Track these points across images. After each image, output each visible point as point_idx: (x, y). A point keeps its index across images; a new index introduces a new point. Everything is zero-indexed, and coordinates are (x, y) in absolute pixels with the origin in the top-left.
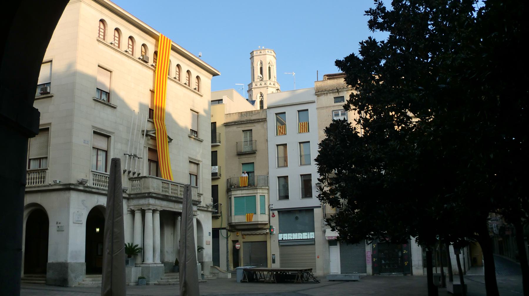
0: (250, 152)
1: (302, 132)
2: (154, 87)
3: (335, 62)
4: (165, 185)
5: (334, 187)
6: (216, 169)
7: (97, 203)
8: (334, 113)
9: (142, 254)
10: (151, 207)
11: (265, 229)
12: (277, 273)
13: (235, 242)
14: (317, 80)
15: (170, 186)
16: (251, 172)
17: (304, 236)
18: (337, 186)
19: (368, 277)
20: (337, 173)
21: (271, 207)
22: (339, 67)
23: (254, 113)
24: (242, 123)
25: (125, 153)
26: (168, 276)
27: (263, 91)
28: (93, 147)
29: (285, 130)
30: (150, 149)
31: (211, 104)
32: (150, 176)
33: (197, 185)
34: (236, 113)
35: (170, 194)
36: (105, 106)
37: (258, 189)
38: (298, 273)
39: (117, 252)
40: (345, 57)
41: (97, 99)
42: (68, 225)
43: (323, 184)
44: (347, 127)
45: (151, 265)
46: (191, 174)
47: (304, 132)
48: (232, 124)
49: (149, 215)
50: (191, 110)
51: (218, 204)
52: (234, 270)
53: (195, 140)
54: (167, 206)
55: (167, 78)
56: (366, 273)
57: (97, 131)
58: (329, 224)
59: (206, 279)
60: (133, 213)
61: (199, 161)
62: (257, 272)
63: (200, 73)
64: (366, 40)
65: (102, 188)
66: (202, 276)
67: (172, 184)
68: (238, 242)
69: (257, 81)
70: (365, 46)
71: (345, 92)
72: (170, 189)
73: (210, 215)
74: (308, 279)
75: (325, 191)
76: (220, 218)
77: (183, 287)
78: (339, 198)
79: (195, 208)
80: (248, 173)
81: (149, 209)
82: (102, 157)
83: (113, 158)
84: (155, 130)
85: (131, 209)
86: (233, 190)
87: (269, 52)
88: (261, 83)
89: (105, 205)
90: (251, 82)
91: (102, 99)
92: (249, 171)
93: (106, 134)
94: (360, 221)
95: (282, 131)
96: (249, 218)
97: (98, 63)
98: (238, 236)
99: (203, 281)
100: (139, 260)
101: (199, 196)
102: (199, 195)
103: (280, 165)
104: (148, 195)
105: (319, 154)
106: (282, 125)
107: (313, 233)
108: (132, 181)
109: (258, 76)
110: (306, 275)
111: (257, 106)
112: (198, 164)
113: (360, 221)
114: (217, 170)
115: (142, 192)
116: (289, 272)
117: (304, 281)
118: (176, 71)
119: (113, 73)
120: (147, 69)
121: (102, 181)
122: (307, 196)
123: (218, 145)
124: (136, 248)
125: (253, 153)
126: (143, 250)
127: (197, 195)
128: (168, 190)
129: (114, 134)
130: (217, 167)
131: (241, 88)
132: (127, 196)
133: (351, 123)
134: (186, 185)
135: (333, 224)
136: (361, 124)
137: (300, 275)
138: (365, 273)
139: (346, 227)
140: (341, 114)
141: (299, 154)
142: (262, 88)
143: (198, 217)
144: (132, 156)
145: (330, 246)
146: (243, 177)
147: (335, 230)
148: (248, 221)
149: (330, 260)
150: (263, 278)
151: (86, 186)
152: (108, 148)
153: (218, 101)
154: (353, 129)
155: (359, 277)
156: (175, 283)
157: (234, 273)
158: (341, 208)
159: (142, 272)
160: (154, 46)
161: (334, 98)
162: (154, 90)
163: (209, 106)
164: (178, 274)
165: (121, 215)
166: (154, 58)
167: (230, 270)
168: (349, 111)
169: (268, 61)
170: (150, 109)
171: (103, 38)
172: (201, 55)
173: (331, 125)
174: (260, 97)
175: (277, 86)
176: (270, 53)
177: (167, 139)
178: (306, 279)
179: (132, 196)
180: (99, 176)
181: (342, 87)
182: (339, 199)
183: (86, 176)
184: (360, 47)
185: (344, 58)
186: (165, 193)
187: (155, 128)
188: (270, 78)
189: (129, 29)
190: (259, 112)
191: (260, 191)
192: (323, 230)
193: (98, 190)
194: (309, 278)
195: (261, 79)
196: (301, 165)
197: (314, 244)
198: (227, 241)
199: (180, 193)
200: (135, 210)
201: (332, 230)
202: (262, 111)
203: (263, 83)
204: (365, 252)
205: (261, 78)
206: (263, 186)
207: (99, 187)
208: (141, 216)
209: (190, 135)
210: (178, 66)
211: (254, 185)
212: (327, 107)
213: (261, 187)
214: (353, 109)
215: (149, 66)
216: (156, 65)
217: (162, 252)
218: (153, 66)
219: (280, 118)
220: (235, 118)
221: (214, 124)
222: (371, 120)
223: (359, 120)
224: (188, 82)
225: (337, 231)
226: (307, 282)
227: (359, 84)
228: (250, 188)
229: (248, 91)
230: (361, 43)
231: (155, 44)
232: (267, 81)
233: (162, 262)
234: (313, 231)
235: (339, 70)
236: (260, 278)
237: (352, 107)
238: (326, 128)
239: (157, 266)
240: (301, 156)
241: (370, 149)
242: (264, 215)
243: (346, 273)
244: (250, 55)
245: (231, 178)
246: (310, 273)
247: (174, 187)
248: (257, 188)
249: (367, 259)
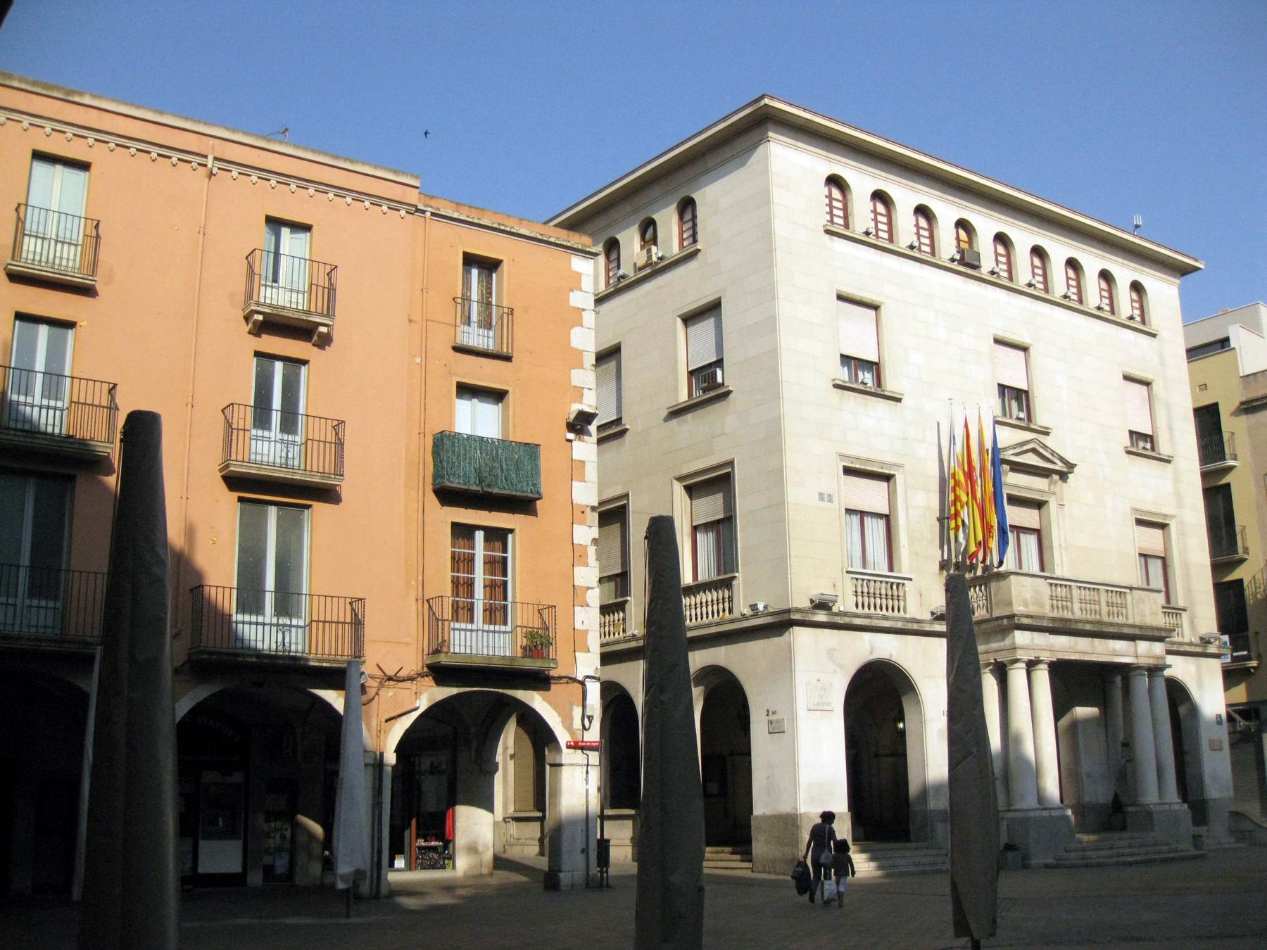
7: (871, 653)
15: (1075, 592)
35: (1078, 615)
42: (793, 718)
45: (1031, 814)
49: (1018, 676)
57: (853, 466)
61: (1165, 516)
65: (881, 613)
67: (1080, 588)
72: (1075, 600)
97: (993, 334)
101: (1177, 614)
102: (1177, 611)
123: (1231, 468)
128: (1097, 607)
129: (902, 469)
183: (834, 586)
186: (1085, 616)
239: (1050, 816)
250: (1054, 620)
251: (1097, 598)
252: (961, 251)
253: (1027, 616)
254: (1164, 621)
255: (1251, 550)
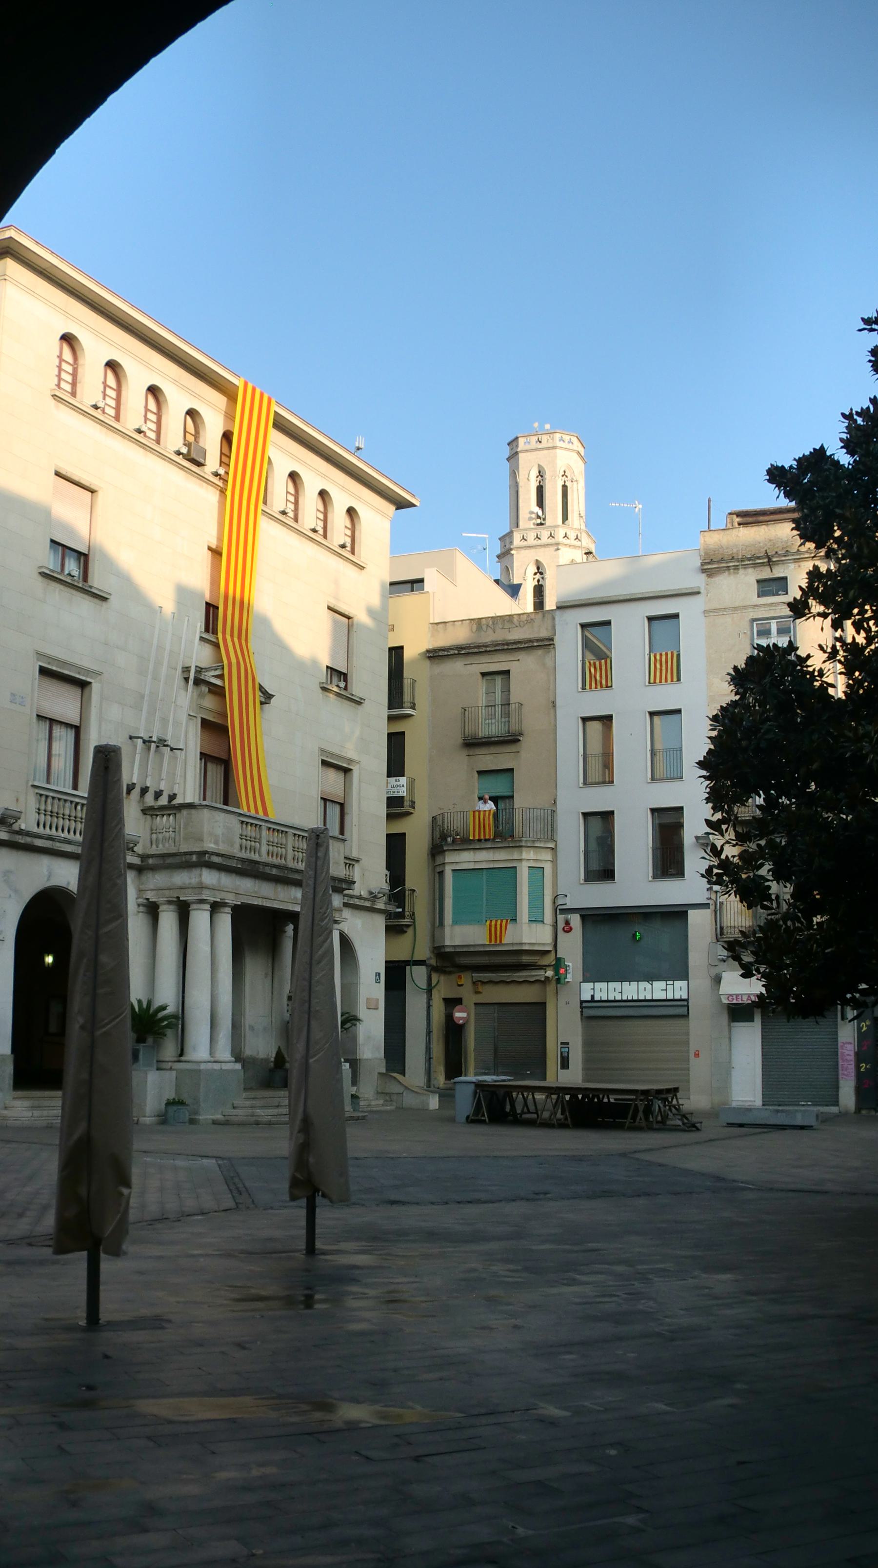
0: (501, 739)
1: (658, 680)
2: (220, 539)
3: (767, 471)
4: (250, 831)
5: (752, 846)
6: (401, 786)
7: (48, 880)
8: (755, 625)
9: (178, 1030)
10: (206, 895)
11: (543, 967)
12: (574, 1096)
13: (452, 1003)
14: (709, 528)
15: (265, 832)
16: (503, 798)
17: (658, 990)
18: (763, 843)
19: (843, 1116)
20: (761, 805)
21: (560, 901)
22: (778, 486)
23: (515, 619)
24: (481, 650)
25: (133, 735)
26: (253, 1098)
27: (544, 556)
28: (38, 716)
29: (608, 673)
30: (205, 723)
31: (390, 594)
32: (204, 803)
33: (342, 832)
34: (462, 621)
35: (264, 858)
36: (74, 592)
37: (523, 848)
38: (635, 1100)
39: (107, 1024)
40: (797, 458)
41: (53, 571)
43: (720, 837)
44: (799, 668)
45: (203, 1067)
46: (325, 800)
47: (666, 680)
48: (452, 652)
49: (200, 919)
50: (329, 608)
51: (404, 890)
52: (449, 1086)
53: (339, 698)
54: (256, 892)
55: (259, 511)
56: (838, 1105)
58: (737, 958)
59: (365, 1109)
60: (152, 910)
61: (350, 761)
62: (514, 1094)
63: (359, 498)
64: (862, 409)
65: (63, 835)
66: (352, 1101)
67: (269, 829)
68: (461, 1004)
69: (527, 526)
70: (859, 425)
71: (792, 566)
72: (264, 842)
73: (380, 922)
74: (665, 1118)
75: (727, 856)
76: (410, 931)
77: (299, 1132)
78: (768, 880)
79: (337, 900)
80: (495, 799)
81: (202, 901)
82: (63, 742)
83: (97, 744)
84: (223, 665)
85: (148, 899)
86: (451, 848)
87: (564, 441)
88: (539, 533)
89: (73, 887)
90: (508, 530)
91: (66, 572)
92: (498, 794)
93: (77, 676)
94: (826, 951)
95: (598, 678)
96: (496, 934)
97: (208, 541)
98: (462, 985)
99: (356, 1114)
100: (169, 1050)
101: (350, 864)
103: (589, 780)
104: (197, 858)
105: (712, 747)
106: (600, 659)
107: (683, 984)
108: (152, 815)
109: (532, 513)
110: (659, 1106)
111: (526, 603)
112: (346, 771)
113: (826, 951)
114: (404, 789)
115: (182, 850)
116: (610, 1096)
117: (655, 1122)
118: (288, 492)
119: (100, 496)
120: (515, 640)
121: (63, 815)
122: (667, 871)
124: (160, 1015)
125: (511, 740)
126: (180, 1022)
127: (342, 861)
129: (99, 677)
130: (403, 780)
131: (480, 547)
132: (136, 861)
133: (809, 657)
134: (313, 831)
135: (748, 958)
136: (840, 661)
137: (641, 1106)
138: (834, 1105)
139: (787, 967)
140: (778, 630)
141: (649, 747)
142: (542, 550)
143: (345, 927)
144: (154, 742)
145: (734, 1024)
146: (479, 811)
147: (754, 975)
148: (493, 943)
149: (733, 1065)
150: (531, 1111)
151: (17, 829)
152: (82, 720)
153: (409, 585)
154: (816, 674)
155: (817, 1116)
156: (274, 1119)
157: (446, 1096)
158: (771, 909)
159: (178, 1087)
160: (223, 416)
161: (758, 581)
162: (222, 549)
163: (384, 598)
164: (284, 1093)
165: (121, 915)
166: (222, 453)
167: (437, 1086)
168: (804, 618)
169: (561, 466)
170: (207, 604)
171: (113, 415)
172: (360, 447)
173: (750, 660)
174: (535, 574)
175: (587, 543)
176: (569, 442)
177: (258, 693)
178: (659, 1118)
179: (151, 861)
180: (56, 801)
181: (783, 549)
182: (767, 884)
183: (17, 800)
184: (843, 425)
185: (795, 459)
186: (249, 855)
187: (223, 662)
188: (565, 517)
189: (147, 365)
190: (532, 619)
191: (528, 855)
192: (713, 975)
193: (51, 842)
194: (668, 1114)
195: (539, 521)
196: (653, 779)
197: (686, 1016)
198: (429, 999)
199: (294, 855)
200: (158, 903)
201: (743, 976)
202: (540, 615)
203: (545, 534)
204: (837, 1045)
205: (539, 517)
206: (539, 840)
207: (53, 832)
208: (178, 923)
209: (326, 683)
210: (294, 476)
211: (512, 836)
212: (735, 609)
213: (533, 841)
214: (819, 615)
215: (206, 477)
216: (227, 473)
217: (236, 1026)
218: (220, 475)
219: (594, 636)
220: (460, 636)
221: (396, 653)
222: (868, 650)
223: (834, 647)
224: (321, 524)
225: (758, 979)
226: (662, 1126)
227: (838, 540)
228: (499, 846)
229: (498, 557)
230: (848, 417)
231: (224, 409)
232: (558, 526)
233: (238, 1056)
234: (684, 975)
235: (778, 497)
236: (523, 1113)
237: (816, 607)
238: (735, 668)
240: (653, 753)
241: (867, 735)
242: (540, 925)
243: (779, 1105)
244: (508, 447)
245: (446, 814)
246: (672, 1099)
247: (276, 838)
248: (521, 846)
249: (840, 1063)
250: (243, 860)
251: (284, 841)
252: (188, 445)
253: (218, 855)
254: (345, 873)
255: (416, 805)
